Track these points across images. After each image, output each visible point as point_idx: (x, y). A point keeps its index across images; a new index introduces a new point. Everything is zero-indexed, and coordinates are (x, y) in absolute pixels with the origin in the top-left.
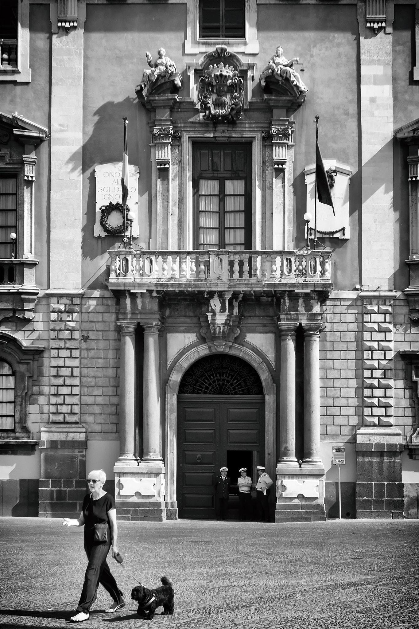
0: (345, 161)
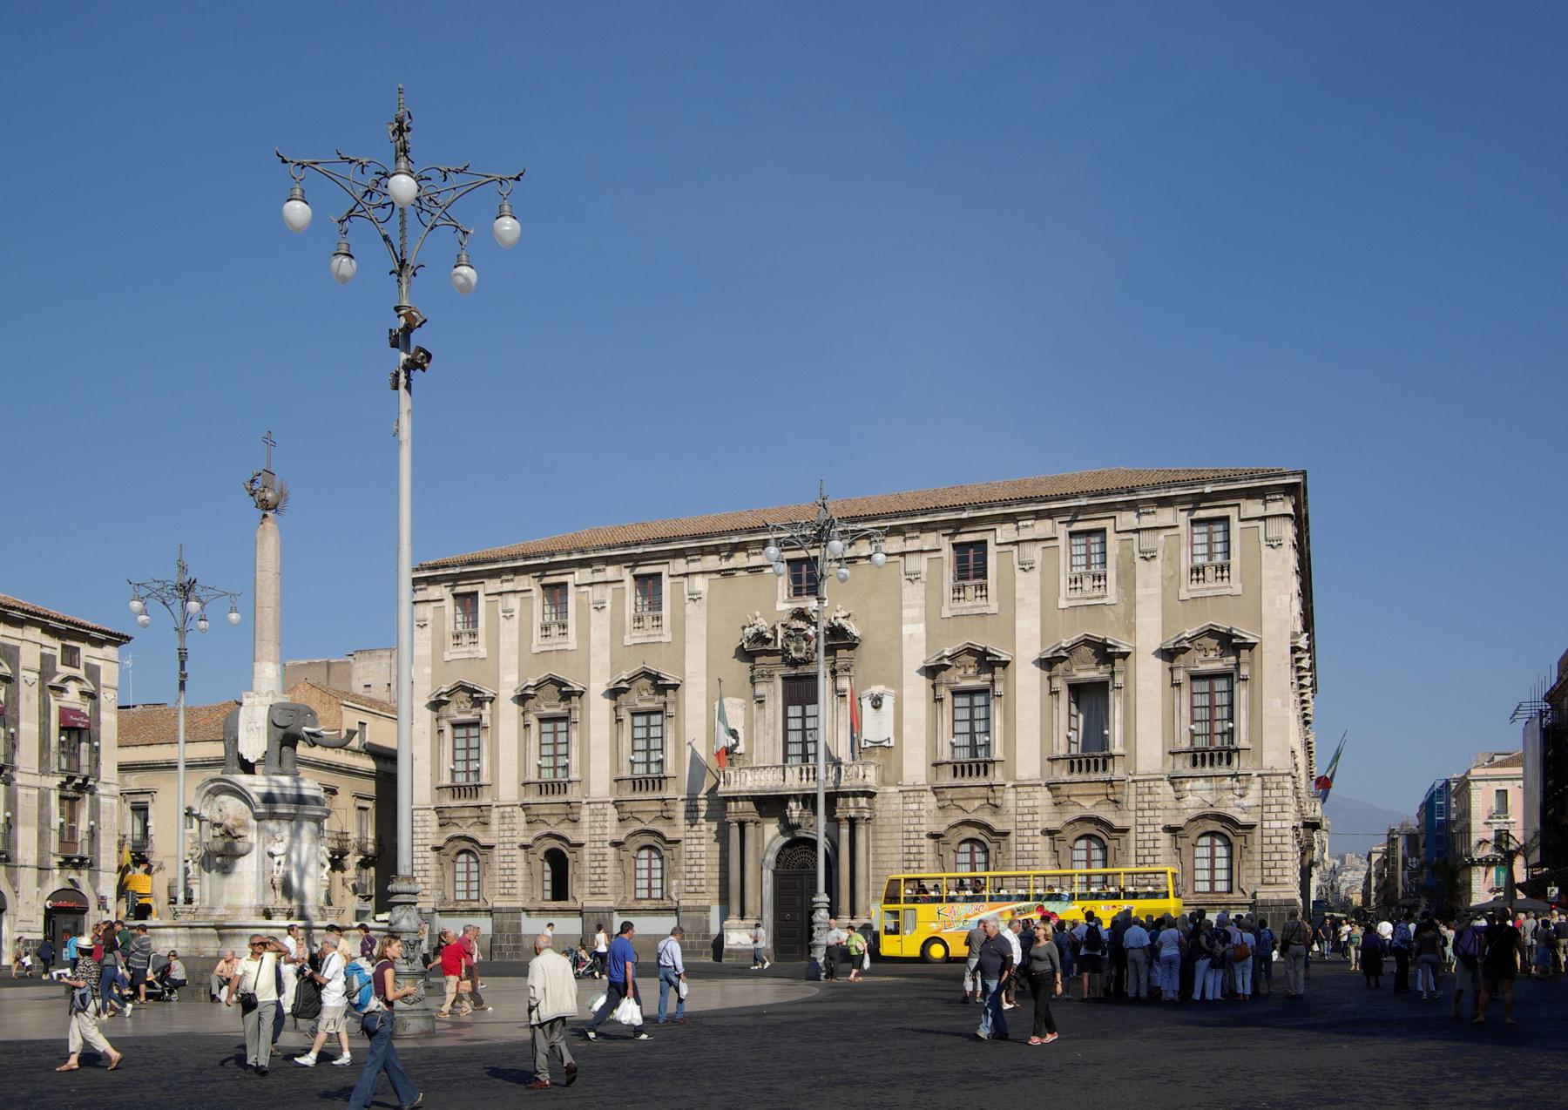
0: (889, 685)
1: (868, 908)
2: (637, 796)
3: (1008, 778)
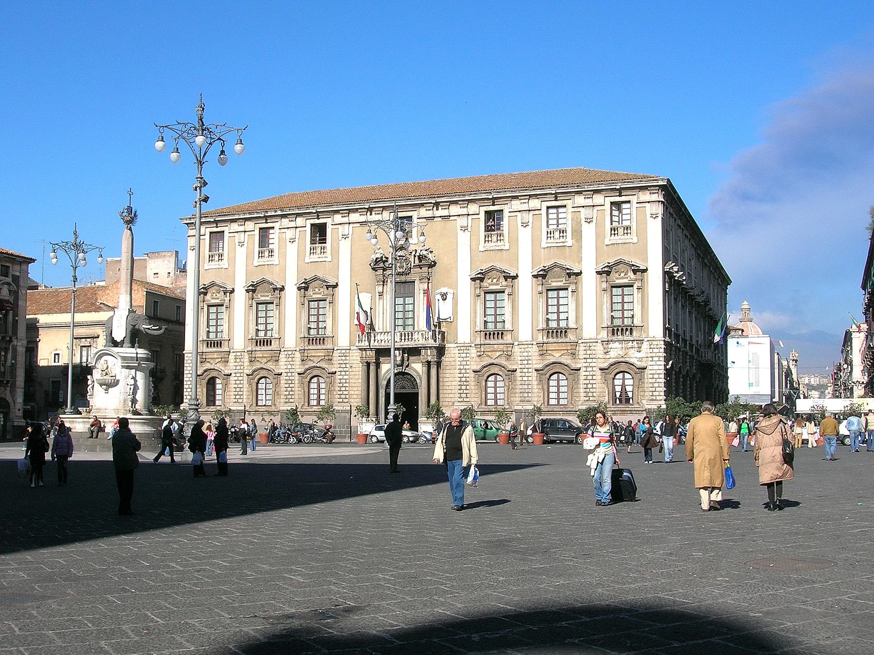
2: (311, 347)
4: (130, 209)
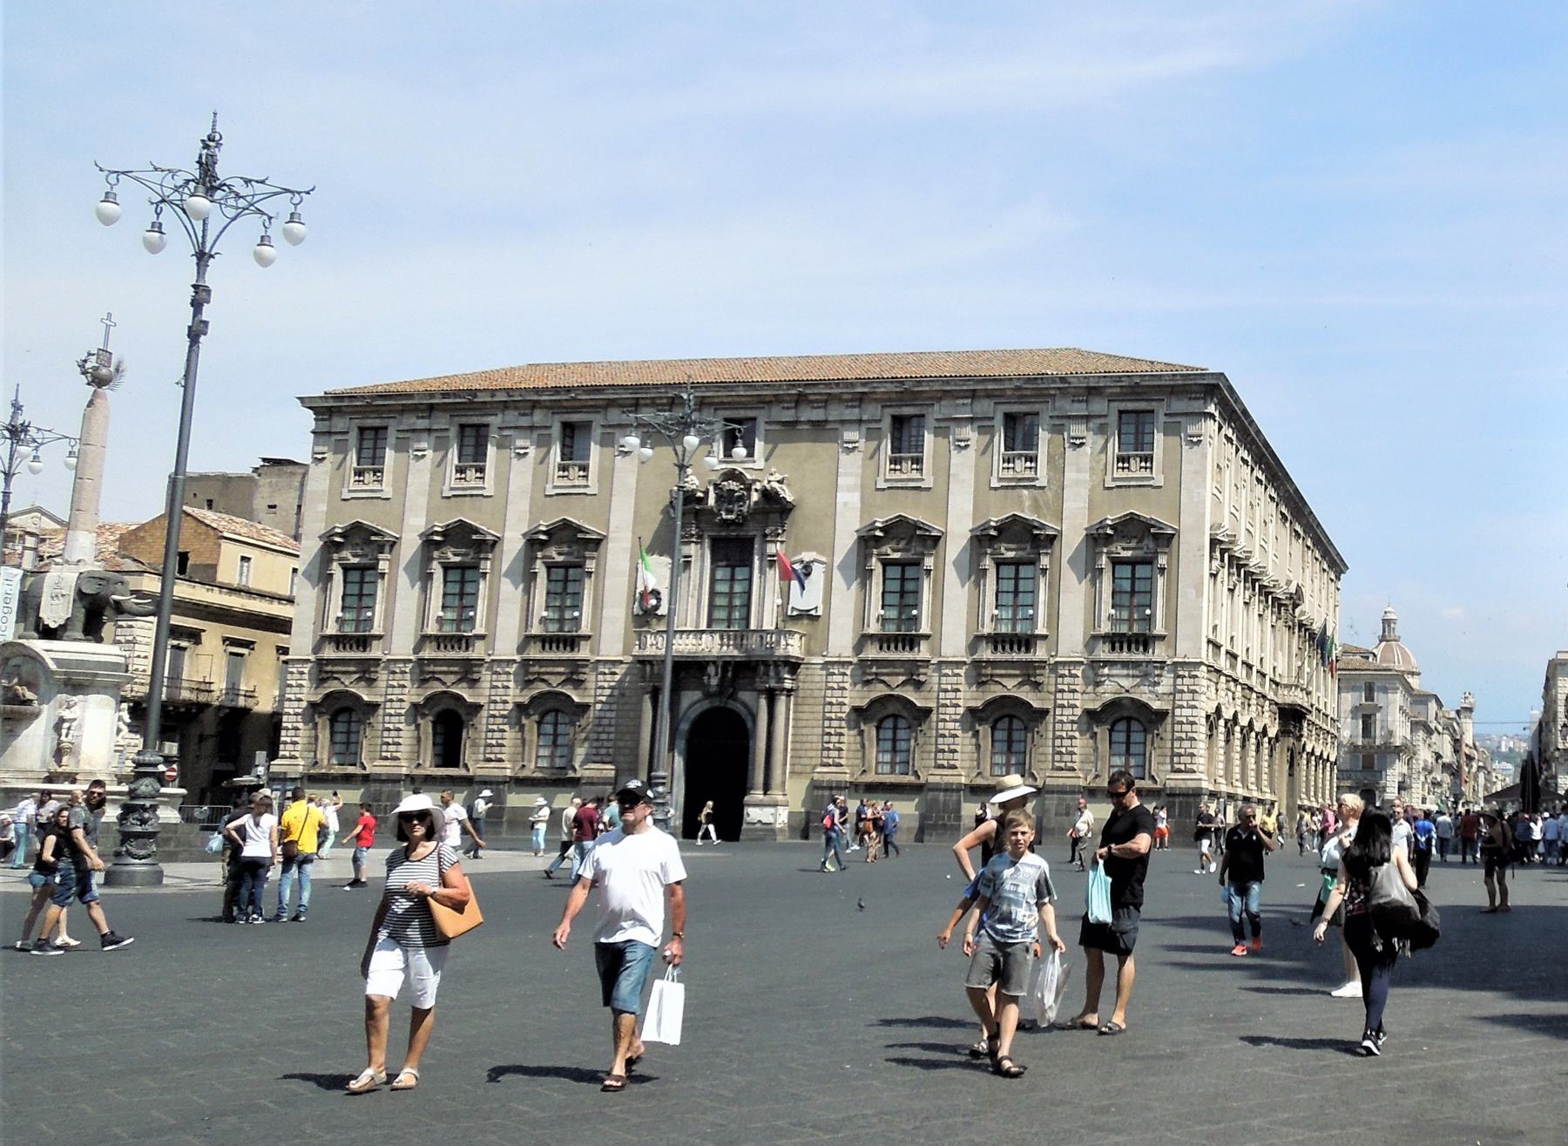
0: (821, 553)
1: (784, 783)
3: (932, 653)
4: (104, 354)
